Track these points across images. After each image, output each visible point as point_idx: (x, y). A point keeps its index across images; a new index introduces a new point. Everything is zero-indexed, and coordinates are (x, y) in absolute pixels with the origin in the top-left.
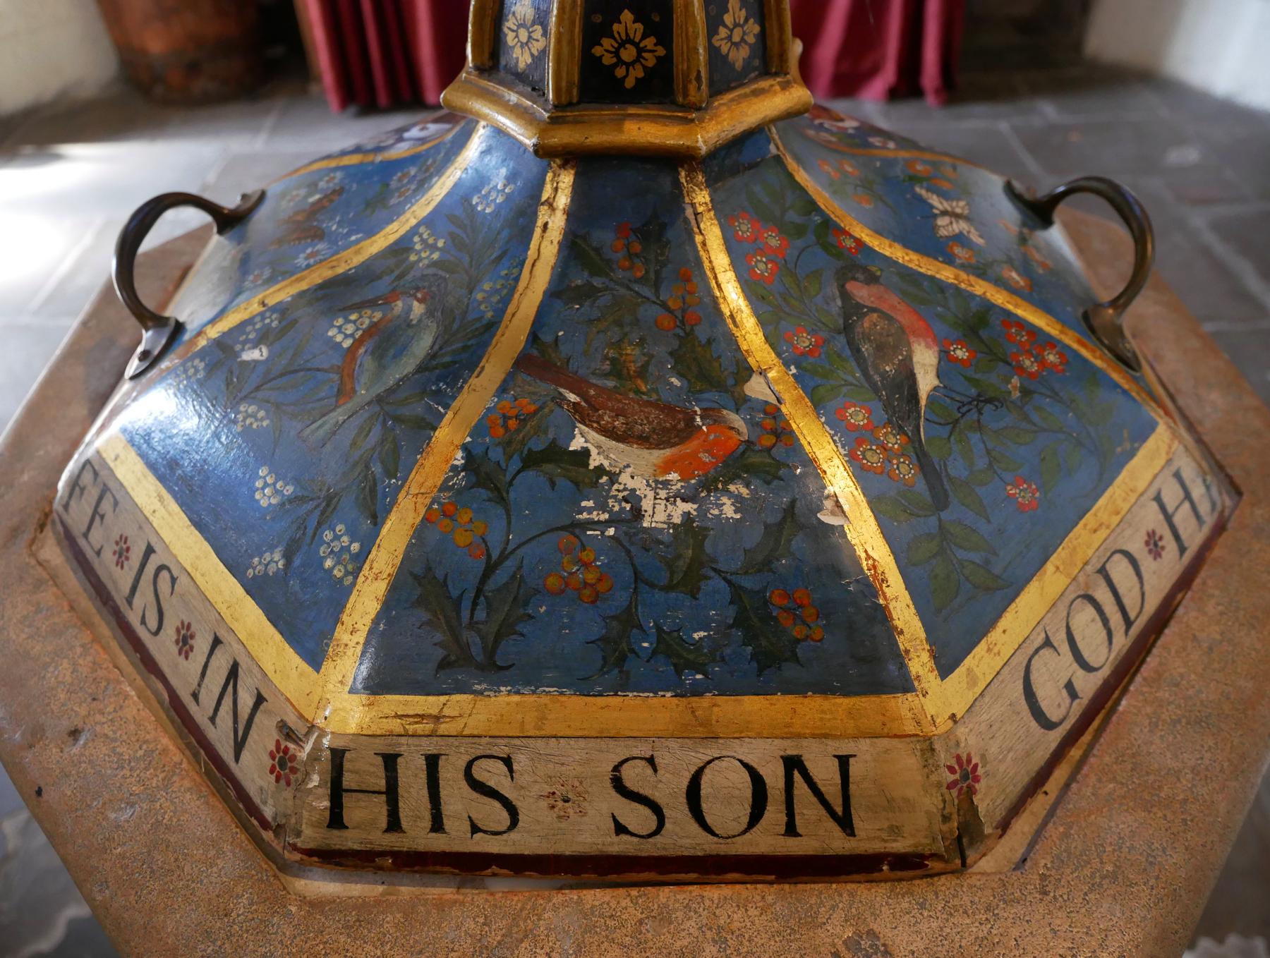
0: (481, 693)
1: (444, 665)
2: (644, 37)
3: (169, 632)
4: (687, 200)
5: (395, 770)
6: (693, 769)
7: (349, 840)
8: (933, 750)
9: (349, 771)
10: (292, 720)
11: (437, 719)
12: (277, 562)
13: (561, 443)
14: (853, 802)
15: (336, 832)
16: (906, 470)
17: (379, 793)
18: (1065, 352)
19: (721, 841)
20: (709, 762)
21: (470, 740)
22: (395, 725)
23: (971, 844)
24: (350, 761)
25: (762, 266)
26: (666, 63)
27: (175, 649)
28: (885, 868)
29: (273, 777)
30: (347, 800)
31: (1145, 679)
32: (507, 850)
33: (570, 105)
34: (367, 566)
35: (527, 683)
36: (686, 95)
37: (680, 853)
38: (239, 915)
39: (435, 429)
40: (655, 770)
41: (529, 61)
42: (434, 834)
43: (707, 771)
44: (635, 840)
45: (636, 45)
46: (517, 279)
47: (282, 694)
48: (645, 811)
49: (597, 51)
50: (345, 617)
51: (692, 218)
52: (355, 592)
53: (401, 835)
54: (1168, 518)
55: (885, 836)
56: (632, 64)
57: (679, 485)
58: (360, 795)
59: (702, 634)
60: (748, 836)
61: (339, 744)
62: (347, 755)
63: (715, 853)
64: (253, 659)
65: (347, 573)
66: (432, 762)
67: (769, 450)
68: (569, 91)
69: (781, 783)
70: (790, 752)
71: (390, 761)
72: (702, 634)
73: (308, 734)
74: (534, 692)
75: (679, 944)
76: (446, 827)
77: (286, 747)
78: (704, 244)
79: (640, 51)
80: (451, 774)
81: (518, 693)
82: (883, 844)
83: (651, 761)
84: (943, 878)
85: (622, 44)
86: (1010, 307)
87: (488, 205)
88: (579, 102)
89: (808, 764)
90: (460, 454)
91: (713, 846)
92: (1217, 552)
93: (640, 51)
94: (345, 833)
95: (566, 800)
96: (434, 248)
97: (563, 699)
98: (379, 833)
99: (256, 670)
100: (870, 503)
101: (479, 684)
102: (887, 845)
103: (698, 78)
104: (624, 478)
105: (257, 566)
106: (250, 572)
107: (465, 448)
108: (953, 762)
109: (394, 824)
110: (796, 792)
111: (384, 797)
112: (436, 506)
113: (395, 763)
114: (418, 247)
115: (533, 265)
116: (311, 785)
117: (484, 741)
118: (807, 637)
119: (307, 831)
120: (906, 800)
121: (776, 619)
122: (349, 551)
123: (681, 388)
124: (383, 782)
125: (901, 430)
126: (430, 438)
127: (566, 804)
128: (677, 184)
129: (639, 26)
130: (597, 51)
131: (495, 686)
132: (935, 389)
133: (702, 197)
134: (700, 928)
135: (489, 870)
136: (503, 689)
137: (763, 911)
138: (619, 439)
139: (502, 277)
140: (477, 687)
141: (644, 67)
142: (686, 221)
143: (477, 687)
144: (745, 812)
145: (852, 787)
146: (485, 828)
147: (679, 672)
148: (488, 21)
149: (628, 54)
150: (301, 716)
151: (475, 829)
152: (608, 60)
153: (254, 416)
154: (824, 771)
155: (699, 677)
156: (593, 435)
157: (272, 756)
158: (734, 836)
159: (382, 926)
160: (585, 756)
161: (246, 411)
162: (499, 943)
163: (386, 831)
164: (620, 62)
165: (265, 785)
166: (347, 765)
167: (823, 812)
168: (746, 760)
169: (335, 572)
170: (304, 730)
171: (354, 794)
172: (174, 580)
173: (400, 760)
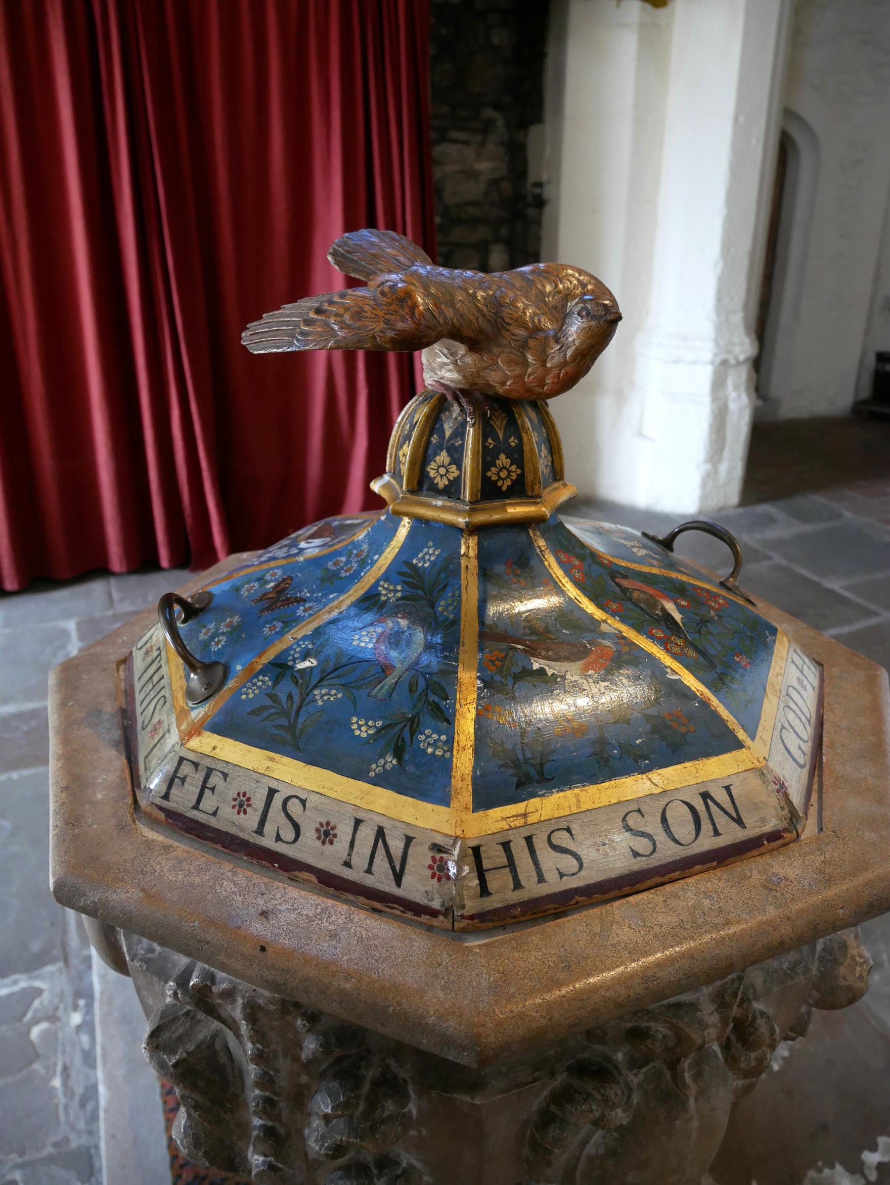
0: (543, 795)
1: (520, 784)
2: (511, 465)
3: (309, 834)
4: (536, 545)
5: (510, 851)
6: (661, 811)
7: (494, 902)
8: (764, 774)
9: (487, 858)
10: (440, 840)
11: (525, 815)
12: (391, 762)
13: (528, 667)
14: (739, 809)
15: (486, 899)
16: (692, 653)
17: (505, 867)
18: (724, 598)
19: (686, 847)
20: (667, 805)
21: (546, 823)
22: (504, 825)
23: (797, 822)
24: (485, 852)
25: (577, 574)
26: (521, 477)
27: (319, 843)
28: (765, 842)
29: (436, 880)
30: (488, 876)
31: (828, 747)
32: (581, 884)
33: (477, 502)
34: (455, 744)
35: (565, 785)
36: (533, 491)
37: (668, 861)
38: (447, 963)
39: (457, 673)
40: (643, 816)
41: (447, 483)
42: (540, 885)
43: (667, 810)
44: (644, 858)
45: (507, 469)
46: (460, 596)
47: (427, 829)
48: (645, 840)
49: (489, 474)
50: (454, 774)
51: (540, 553)
52: (455, 760)
53: (523, 890)
54: (802, 671)
55: (759, 824)
56: (506, 479)
57: (596, 675)
58: (495, 871)
59: (640, 740)
60: (697, 841)
61: (474, 843)
62: (481, 849)
63: (684, 856)
64: (394, 819)
65: (445, 752)
66: (529, 840)
67: (629, 652)
68: (477, 496)
69: (703, 808)
70: (702, 790)
71: (506, 846)
72: (640, 740)
73: (454, 845)
74: (570, 789)
75: (690, 904)
76: (546, 878)
77: (441, 857)
78: (549, 565)
79: (509, 472)
80: (540, 844)
81: (562, 791)
82: (760, 829)
83: (639, 811)
84: (791, 845)
85: (501, 470)
86: (691, 581)
87: (425, 562)
88: (481, 500)
89: (712, 795)
90: (479, 682)
91: (683, 852)
92: (826, 690)
93: (509, 472)
94: (492, 898)
95: (604, 845)
96: (395, 591)
97: (585, 788)
98: (510, 892)
99: (399, 825)
100: (685, 668)
101: (541, 791)
102: (762, 829)
103: (540, 482)
104: (568, 676)
105: (375, 769)
106: (372, 774)
107: (478, 678)
108: (774, 779)
109: (517, 885)
110: (712, 811)
111: (508, 869)
112: (480, 708)
113: (509, 847)
114: (384, 592)
115: (466, 588)
116: (464, 874)
117: (553, 821)
118: (688, 732)
119: (468, 903)
120: (762, 802)
121: (670, 726)
122: (441, 741)
123: (570, 634)
124: (505, 859)
125: (680, 638)
126: (457, 678)
127: (605, 847)
128: (529, 536)
129: (509, 461)
130: (489, 474)
131: (549, 791)
132: (682, 618)
133: (542, 543)
134: (695, 895)
135: (574, 900)
136: (554, 790)
137: (720, 880)
138: (555, 660)
139: (450, 597)
140: (541, 793)
141: (511, 480)
142: (537, 554)
143: (541, 793)
144: (692, 827)
145: (736, 801)
146: (567, 873)
147: (636, 761)
148: (418, 466)
149: (503, 474)
150: (446, 835)
151: (562, 875)
152: (494, 478)
153: (329, 694)
154: (721, 796)
155: (647, 762)
156: (541, 661)
157: (431, 867)
158: (691, 843)
159: (533, 942)
160: (606, 817)
161: (320, 693)
162: (601, 930)
163: (514, 890)
164: (500, 478)
165: (429, 888)
166: (483, 855)
167: (728, 818)
168: (684, 799)
169: (437, 753)
170: (451, 841)
171: (491, 871)
172: (303, 802)
173: (511, 844)
